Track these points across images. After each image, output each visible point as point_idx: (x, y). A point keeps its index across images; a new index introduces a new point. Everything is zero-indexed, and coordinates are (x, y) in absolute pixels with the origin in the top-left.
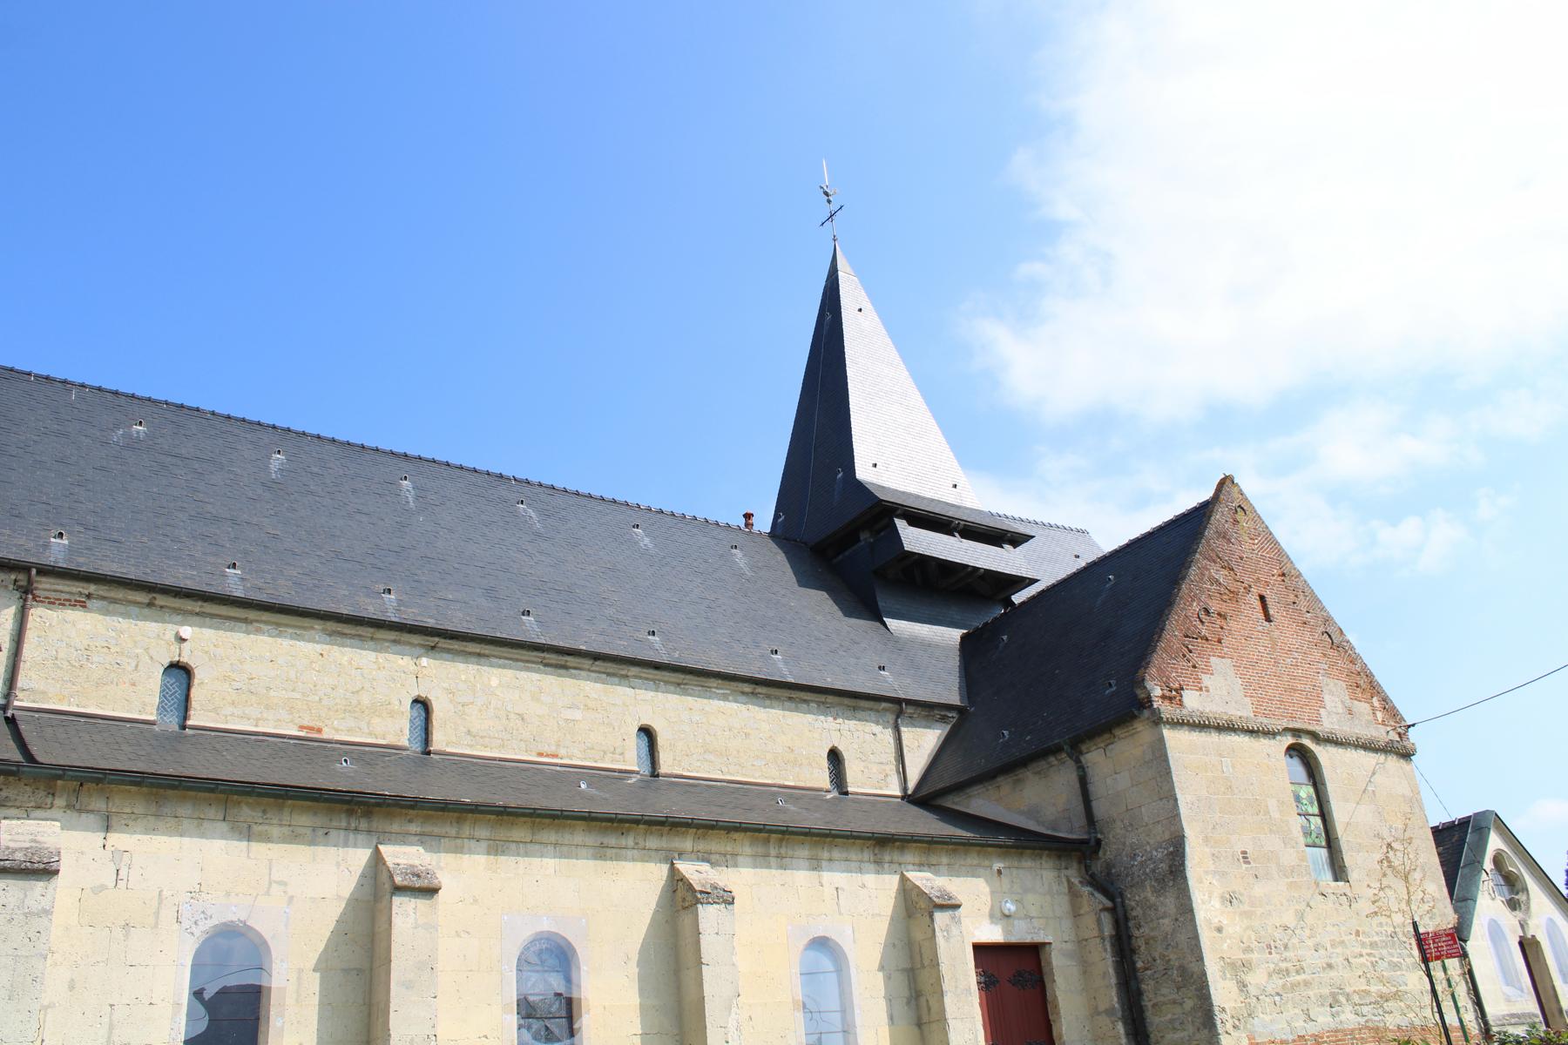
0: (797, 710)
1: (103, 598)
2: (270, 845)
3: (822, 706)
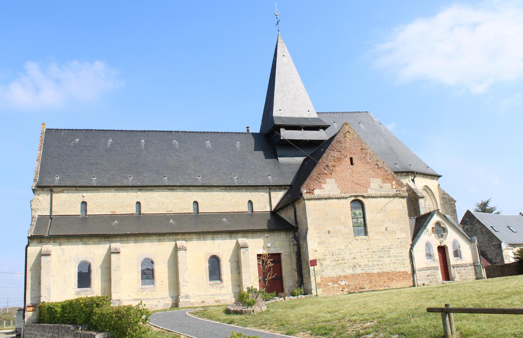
0: (239, 192)
1: (67, 190)
2: (90, 245)
3: (246, 190)
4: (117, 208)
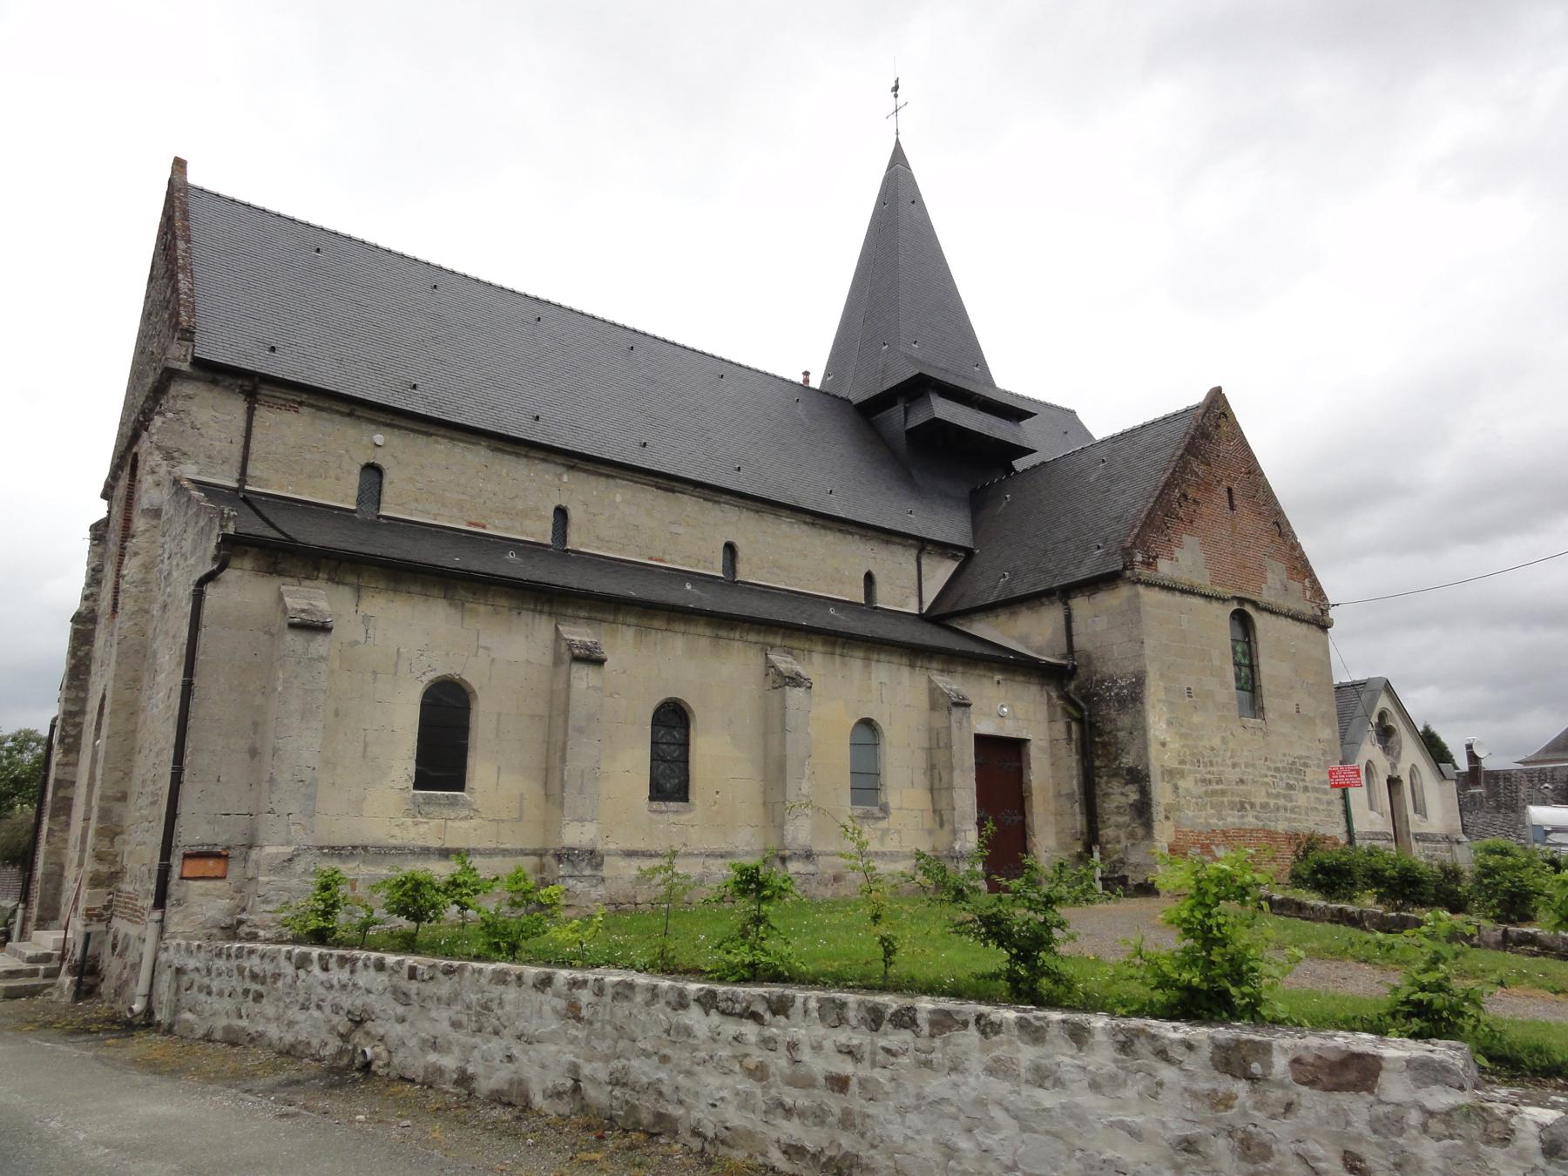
4: (493, 514)
